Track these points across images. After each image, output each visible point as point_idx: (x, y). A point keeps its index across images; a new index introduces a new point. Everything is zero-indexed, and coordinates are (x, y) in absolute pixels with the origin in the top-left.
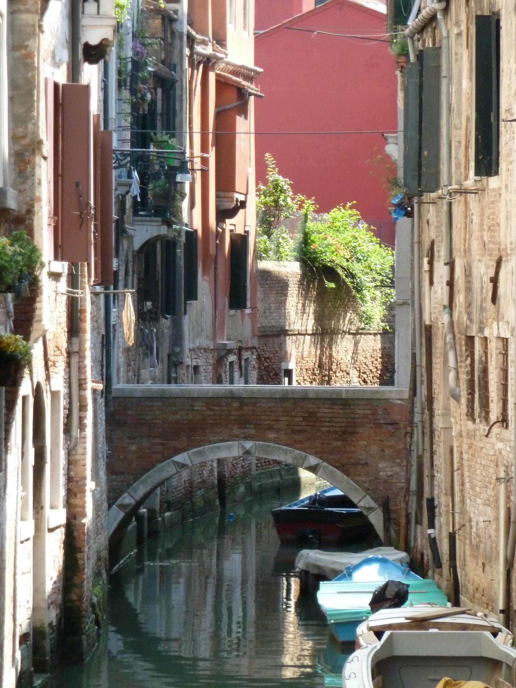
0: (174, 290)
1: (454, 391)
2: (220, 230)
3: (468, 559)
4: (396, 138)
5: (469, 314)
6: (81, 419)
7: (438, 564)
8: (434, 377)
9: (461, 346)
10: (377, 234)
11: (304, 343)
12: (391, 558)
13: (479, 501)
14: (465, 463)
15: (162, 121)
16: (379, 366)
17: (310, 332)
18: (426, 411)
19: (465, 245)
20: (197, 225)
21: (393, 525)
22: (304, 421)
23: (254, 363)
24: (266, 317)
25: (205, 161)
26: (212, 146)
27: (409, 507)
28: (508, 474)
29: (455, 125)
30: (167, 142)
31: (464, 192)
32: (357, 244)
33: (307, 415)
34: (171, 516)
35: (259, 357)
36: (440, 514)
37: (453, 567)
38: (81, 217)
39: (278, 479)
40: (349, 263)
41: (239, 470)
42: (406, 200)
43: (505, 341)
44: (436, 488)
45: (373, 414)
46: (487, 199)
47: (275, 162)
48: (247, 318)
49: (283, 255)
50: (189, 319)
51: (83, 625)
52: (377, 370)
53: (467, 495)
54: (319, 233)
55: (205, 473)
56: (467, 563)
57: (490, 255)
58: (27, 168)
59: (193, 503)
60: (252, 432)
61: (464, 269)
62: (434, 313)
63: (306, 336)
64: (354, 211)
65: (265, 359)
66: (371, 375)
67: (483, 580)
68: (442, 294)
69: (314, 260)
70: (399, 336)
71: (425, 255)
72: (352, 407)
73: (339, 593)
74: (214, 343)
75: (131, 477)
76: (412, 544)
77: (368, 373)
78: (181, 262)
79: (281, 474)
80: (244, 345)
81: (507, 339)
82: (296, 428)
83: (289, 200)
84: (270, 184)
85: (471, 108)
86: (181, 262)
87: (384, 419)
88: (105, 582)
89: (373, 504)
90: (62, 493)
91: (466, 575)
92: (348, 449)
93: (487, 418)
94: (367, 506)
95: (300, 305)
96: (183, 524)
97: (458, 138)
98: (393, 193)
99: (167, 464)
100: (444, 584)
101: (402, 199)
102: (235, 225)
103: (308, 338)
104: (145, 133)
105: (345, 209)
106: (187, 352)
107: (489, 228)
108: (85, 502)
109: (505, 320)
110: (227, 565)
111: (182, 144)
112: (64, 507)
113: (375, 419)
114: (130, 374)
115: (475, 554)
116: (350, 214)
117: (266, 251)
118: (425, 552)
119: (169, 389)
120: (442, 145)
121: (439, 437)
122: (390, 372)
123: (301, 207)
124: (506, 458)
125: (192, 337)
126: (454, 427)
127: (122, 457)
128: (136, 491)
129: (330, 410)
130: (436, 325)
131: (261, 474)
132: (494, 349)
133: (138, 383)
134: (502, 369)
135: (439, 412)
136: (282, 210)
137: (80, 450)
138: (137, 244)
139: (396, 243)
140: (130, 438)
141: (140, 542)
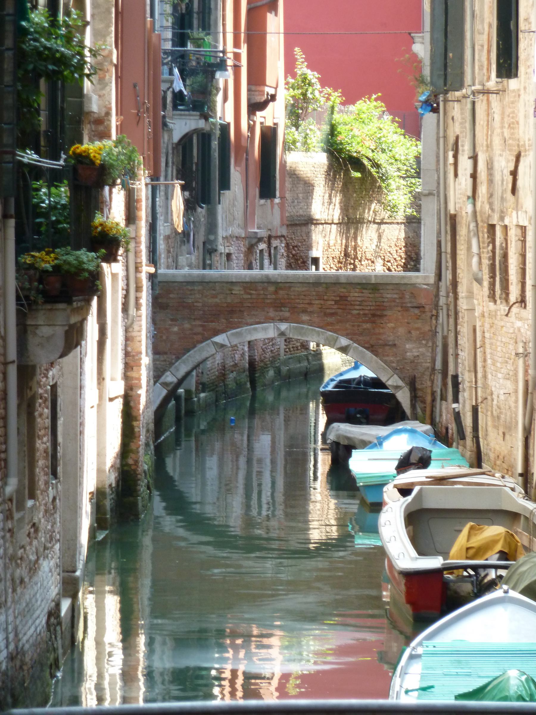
0: (209, 180)
1: (477, 274)
2: (252, 123)
3: (490, 429)
4: (423, 38)
5: (491, 204)
6: (137, 299)
7: (462, 436)
8: (459, 262)
9: (483, 234)
10: (402, 125)
11: (330, 231)
12: (419, 430)
13: (500, 375)
14: (487, 341)
15: (199, 20)
16: (403, 255)
17: (336, 221)
18: (451, 294)
19: (487, 140)
20: (230, 118)
21: (419, 402)
22: (335, 304)
23: (283, 251)
24: (294, 207)
25: (237, 56)
26: (244, 43)
27: (435, 386)
28: (526, 350)
29: (478, 30)
30: (204, 39)
31: (487, 92)
32: (382, 135)
33: (338, 298)
34: (206, 397)
35: (287, 246)
36: (464, 390)
37: (476, 437)
38: (138, 115)
39: (305, 364)
40: (374, 154)
41: (268, 355)
42: (433, 98)
43: (523, 229)
44: (460, 365)
45: (401, 298)
46: (508, 99)
47: (304, 56)
48: (276, 207)
49: (310, 146)
50: (223, 208)
51: (138, 487)
52: (402, 258)
53: (488, 370)
54: (345, 124)
55: (237, 357)
56: (488, 433)
57: (510, 150)
58: (105, 76)
59: (225, 385)
60: (287, 314)
61: (486, 163)
62: (459, 203)
63: (333, 225)
64: (379, 103)
65: (293, 247)
66: (396, 264)
67: (503, 448)
68: (466, 185)
69: (340, 151)
70: (424, 225)
71: (450, 149)
72: (381, 291)
73: (369, 460)
74: (246, 232)
75: (174, 357)
76: (437, 420)
77: (392, 262)
78: (215, 154)
79: (308, 359)
80: (274, 234)
81: (525, 227)
82: (328, 311)
83: (317, 93)
84: (298, 77)
85: (493, 16)
86: (215, 154)
87: (410, 302)
88: (153, 452)
89: (400, 383)
90: (120, 366)
91: (488, 445)
92: (377, 331)
93: (507, 300)
94: (395, 384)
95: (327, 195)
96: (217, 406)
97: (481, 42)
98: (420, 91)
99: (207, 344)
100: (468, 454)
101: (429, 96)
102: (265, 118)
103: (334, 227)
104: (181, 29)
105: (370, 101)
106: (220, 240)
107: (509, 126)
108: (141, 375)
109: (524, 209)
110: (257, 446)
111: (216, 40)
112: (122, 379)
113: (403, 303)
114: (170, 260)
115: (496, 424)
116: (375, 106)
117: (294, 142)
118: (450, 426)
119: (208, 274)
120: (466, 47)
121: (463, 318)
122: (413, 261)
123: (328, 99)
124: (524, 335)
125: (225, 225)
126: (476, 308)
127: (164, 337)
128: (178, 370)
129: (360, 295)
130: (460, 214)
131: (289, 358)
132: (513, 236)
133: (176, 269)
134: (521, 254)
135: (463, 294)
136: (310, 103)
137: (136, 327)
138: (176, 137)
139: (422, 136)
140: (172, 320)
141: (178, 419)
